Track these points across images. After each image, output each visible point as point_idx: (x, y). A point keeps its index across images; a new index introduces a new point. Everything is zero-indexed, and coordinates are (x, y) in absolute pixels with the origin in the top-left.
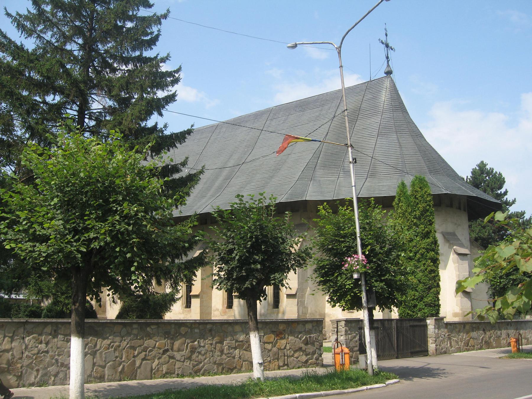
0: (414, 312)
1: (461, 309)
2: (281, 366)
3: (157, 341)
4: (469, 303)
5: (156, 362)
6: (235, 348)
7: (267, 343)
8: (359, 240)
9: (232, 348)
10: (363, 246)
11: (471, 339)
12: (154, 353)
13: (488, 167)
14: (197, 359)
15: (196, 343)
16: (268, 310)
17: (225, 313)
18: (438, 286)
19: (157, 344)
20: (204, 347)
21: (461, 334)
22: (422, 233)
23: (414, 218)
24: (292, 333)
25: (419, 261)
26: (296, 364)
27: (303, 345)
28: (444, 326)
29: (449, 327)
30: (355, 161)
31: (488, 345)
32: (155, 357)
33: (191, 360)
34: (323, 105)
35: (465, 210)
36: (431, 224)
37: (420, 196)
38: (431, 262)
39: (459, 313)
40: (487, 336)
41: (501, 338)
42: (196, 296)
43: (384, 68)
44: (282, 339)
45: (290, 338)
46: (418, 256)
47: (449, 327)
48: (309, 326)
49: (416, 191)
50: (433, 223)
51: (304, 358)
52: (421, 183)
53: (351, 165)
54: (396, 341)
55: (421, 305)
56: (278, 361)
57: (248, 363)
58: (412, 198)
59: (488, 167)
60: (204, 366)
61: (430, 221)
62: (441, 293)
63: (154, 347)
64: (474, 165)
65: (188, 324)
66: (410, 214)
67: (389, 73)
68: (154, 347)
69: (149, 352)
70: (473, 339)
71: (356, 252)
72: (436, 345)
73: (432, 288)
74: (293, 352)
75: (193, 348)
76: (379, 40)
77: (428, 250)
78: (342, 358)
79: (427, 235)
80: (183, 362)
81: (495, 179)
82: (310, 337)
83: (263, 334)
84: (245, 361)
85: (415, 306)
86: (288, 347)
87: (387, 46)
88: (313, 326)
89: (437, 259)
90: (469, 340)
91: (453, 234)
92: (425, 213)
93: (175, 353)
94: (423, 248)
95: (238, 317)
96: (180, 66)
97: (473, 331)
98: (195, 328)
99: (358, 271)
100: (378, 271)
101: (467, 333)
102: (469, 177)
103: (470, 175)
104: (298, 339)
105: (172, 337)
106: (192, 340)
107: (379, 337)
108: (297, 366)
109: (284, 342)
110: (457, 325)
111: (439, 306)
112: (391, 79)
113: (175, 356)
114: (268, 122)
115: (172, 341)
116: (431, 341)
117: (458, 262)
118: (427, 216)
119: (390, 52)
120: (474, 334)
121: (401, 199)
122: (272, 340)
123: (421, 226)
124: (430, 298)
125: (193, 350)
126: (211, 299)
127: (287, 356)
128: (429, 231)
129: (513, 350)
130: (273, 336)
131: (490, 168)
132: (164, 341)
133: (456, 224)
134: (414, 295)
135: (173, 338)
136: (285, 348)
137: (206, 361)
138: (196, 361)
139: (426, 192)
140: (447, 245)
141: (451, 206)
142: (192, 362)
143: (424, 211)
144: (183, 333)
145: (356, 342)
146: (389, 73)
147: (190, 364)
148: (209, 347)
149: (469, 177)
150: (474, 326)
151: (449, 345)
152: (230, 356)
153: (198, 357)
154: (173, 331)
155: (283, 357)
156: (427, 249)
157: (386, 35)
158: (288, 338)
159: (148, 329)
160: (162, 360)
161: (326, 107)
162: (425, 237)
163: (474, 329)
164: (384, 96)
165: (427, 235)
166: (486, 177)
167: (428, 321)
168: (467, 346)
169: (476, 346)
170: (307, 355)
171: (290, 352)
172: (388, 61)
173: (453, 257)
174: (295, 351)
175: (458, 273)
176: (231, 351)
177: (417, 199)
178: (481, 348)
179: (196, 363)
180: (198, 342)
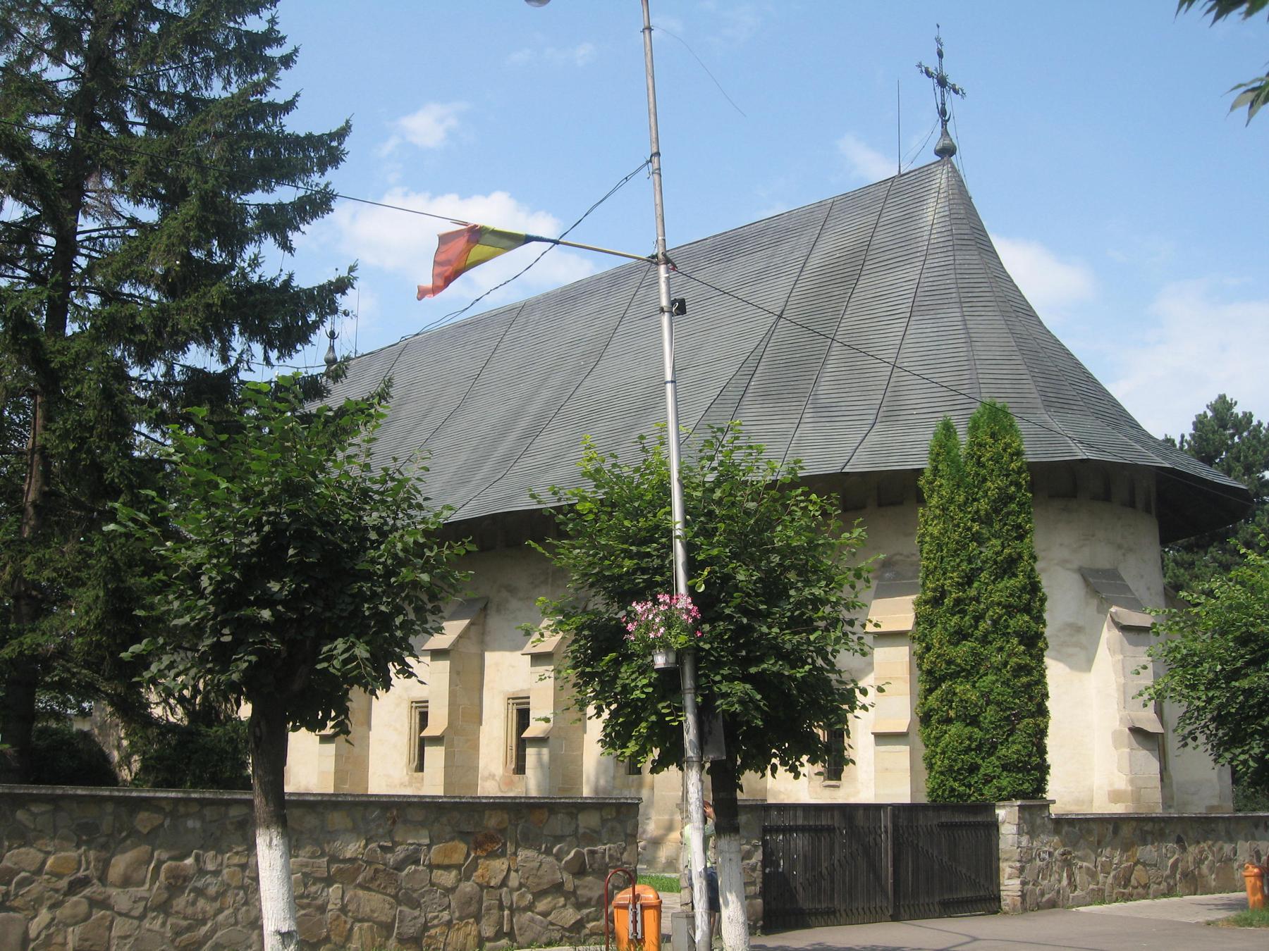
0: (969, 786)
1: (1132, 781)
2: (489, 939)
3: (48, 853)
4: (1155, 766)
5: (44, 916)
6: (329, 881)
7: (439, 867)
8: (679, 548)
9: (317, 880)
10: (692, 568)
11: (1139, 867)
12: (35, 888)
13: (1238, 410)
14: (190, 911)
15: (189, 861)
16: (614, 778)
17: (510, 784)
18: (1042, 712)
19: (49, 862)
20: (216, 873)
21: (1107, 851)
22: (995, 562)
23: (973, 520)
24: (528, 840)
25: (984, 641)
26: (540, 934)
27: (567, 877)
28: (1051, 826)
29: (1066, 829)
30: (679, 307)
31: (1193, 883)
32: (39, 901)
33: (167, 914)
34: (778, 242)
35: (1148, 510)
36: (1021, 538)
37: (991, 459)
38: (1020, 643)
39: (1125, 792)
40: (1190, 859)
41: (1236, 865)
42: (436, 740)
43: (935, 141)
44: (492, 855)
45: (523, 854)
46: (985, 625)
47: (1066, 829)
48: (588, 821)
49: (980, 445)
50: (1026, 532)
51: (570, 916)
52: (996, 421)
53: (665, 319)
54: (890, 870)
55: (988, 766)
56: (478, 921)
57: (371, 928)
58: (970, 463)
59: (1238, 410)
60: (214, 931)
61: (1019, 526)
62: (1049, 731)
63: (39, 871)
64: (1199, 403)
65: (164, 804)
66: (961, 507)
67: (946, 152)
68: (39, 871)
69: (21, 884)
70: (1144, 864)
71: (669, 586)
72: (1023, 883)
73: (1024, 717)
74: (530, 897)
75: (176, 877)
76: (920, 66)
77: (1011, 610)
78: (635, 922)
79: (1008, 567)
80: (142, 917)
81: (1254, 442)
82: (592, 853)
83: (427, 841)
84: (362, 920)
85: (974, 769)
86: (514, 880)
87: (942, 82)
88: (604, 821)
89: (1039, 636)
90: (1131, 870)
91: (1112, 575)
92: (1005, 505)
93: (114, 892)
94: (999, 604)
95: (533, 793)
96: (347, 122)
97: (1145, 843)
98: (187, 815)
99: (667, 647)
100: (739, 647)
101: (1127, 847)
102: (1188, 438)
103: (1188, 430)
104: (551, 859)
105: (103, 840)
106: (173, 853)
107: (836, 857)
108: (544, 939)
109: (500, 865)
110: (1093, 826)
111: (1044, 769)
112: (953, 167)
113: (112, 901)
114: (642, 291)
115: (104, 854)
116: (1008, 870)
117: (1122, 651)
118: (1009, 514)
119: (951, 99)
120: (1148, 852)
121: (940, 467)
122: (458, 858)
123: (994, 541)
124: (1015, 747)
125: (177, 883)
126: (476, 747)
127: (511, 908)
128: (1015, 556)
129: (1251, 900)
130: (463, 847)
131: (1245, 414)
132: (73, 854)
133: (1120, 547)
134: (970, 738)
135: (110, 846)
136: (504, 883)
137: (221, 917)
138: (185, 918)
139: (1007, 446)
140: (1094, 602)
141: (1106, 496)
142: (171, 920)
143: (1000, 499)
144: (145, 831)
145: (753, 869)
146: (946, 152)
147: (164, 924)
148: (233, 875)
149: (1188, 438)
150: (1148, 827)
151: (1065, 882)
152: (309, 905)
153: (194, 903)
154: (107, 824)
155: (495, 911)
156: (1008, 607)
157: (940, 55)
158: (515, 854)
159: (20, 815)
160: (64, 912)
161: (786, 247)
162: (1005, 572)
163: (1149, 838)
164: (933, 213)
165: (1008, 567)
166: (1232, 436)
167: (1001, 813)
168: (1125, 886)
169: (1154, 887)
170: (579, 906)
171: (522, 896)
172: (944, 123)
173: (1109, 635)
174: (539, 895)
175: (1122, 680)
176: (313, 889)
177: (984, 466)
178: (1169, 893)
179: (185, 923)
180: (197, 859)
